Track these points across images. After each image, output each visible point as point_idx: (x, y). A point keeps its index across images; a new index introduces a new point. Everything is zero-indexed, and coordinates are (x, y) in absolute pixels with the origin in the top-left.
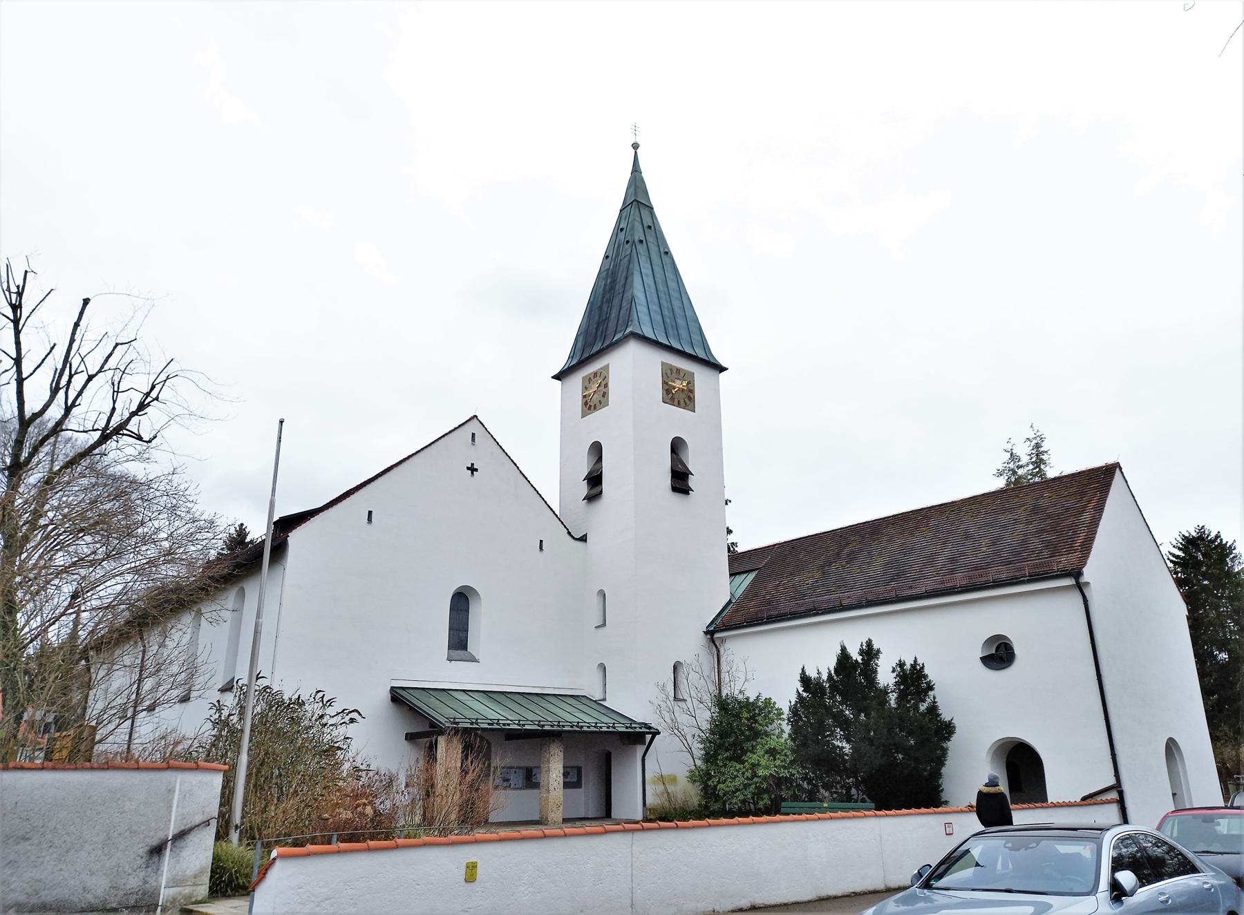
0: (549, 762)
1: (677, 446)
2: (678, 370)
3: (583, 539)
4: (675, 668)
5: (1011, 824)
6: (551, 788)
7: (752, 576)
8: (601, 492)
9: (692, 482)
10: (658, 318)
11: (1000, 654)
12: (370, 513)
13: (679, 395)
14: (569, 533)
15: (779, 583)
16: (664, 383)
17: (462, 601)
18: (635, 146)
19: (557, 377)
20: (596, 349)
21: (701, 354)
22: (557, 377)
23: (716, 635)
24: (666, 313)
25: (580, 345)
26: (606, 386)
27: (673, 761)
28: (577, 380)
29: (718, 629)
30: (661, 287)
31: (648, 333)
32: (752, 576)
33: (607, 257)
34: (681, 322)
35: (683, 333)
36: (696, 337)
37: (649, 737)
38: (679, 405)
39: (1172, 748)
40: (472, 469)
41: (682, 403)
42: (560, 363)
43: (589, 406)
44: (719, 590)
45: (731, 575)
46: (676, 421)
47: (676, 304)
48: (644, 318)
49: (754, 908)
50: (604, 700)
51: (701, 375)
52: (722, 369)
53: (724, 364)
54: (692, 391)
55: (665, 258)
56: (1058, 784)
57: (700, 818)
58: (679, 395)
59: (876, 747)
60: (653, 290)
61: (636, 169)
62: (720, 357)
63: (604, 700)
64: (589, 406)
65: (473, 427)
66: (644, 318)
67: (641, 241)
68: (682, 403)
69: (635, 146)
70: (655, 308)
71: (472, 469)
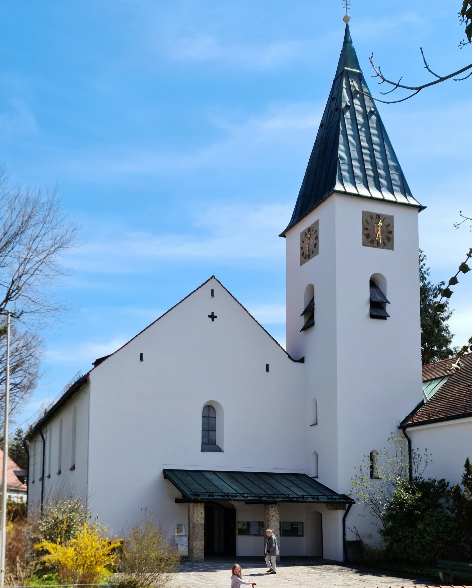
3: (302, 360)
5: (277, 566)
8: (313, 324)
9: (389, 309)
14: (290, 357)
16: (365, 229)
17: (267, 366)
19: (283, 235)
22: (283, 235)
23: (408, 430)
26: (317, 238)
27: (362, 523)
37: (347, 505)
38: (378, 245)
40: (213, 317)
46: (376, 260)
50: (317, 477)
56: (242, 523)
58: (378, 233)
61: (347, 41)
63: (317, 477)
65: (213, 285)
69: (346, 19)
71: (213, 317)
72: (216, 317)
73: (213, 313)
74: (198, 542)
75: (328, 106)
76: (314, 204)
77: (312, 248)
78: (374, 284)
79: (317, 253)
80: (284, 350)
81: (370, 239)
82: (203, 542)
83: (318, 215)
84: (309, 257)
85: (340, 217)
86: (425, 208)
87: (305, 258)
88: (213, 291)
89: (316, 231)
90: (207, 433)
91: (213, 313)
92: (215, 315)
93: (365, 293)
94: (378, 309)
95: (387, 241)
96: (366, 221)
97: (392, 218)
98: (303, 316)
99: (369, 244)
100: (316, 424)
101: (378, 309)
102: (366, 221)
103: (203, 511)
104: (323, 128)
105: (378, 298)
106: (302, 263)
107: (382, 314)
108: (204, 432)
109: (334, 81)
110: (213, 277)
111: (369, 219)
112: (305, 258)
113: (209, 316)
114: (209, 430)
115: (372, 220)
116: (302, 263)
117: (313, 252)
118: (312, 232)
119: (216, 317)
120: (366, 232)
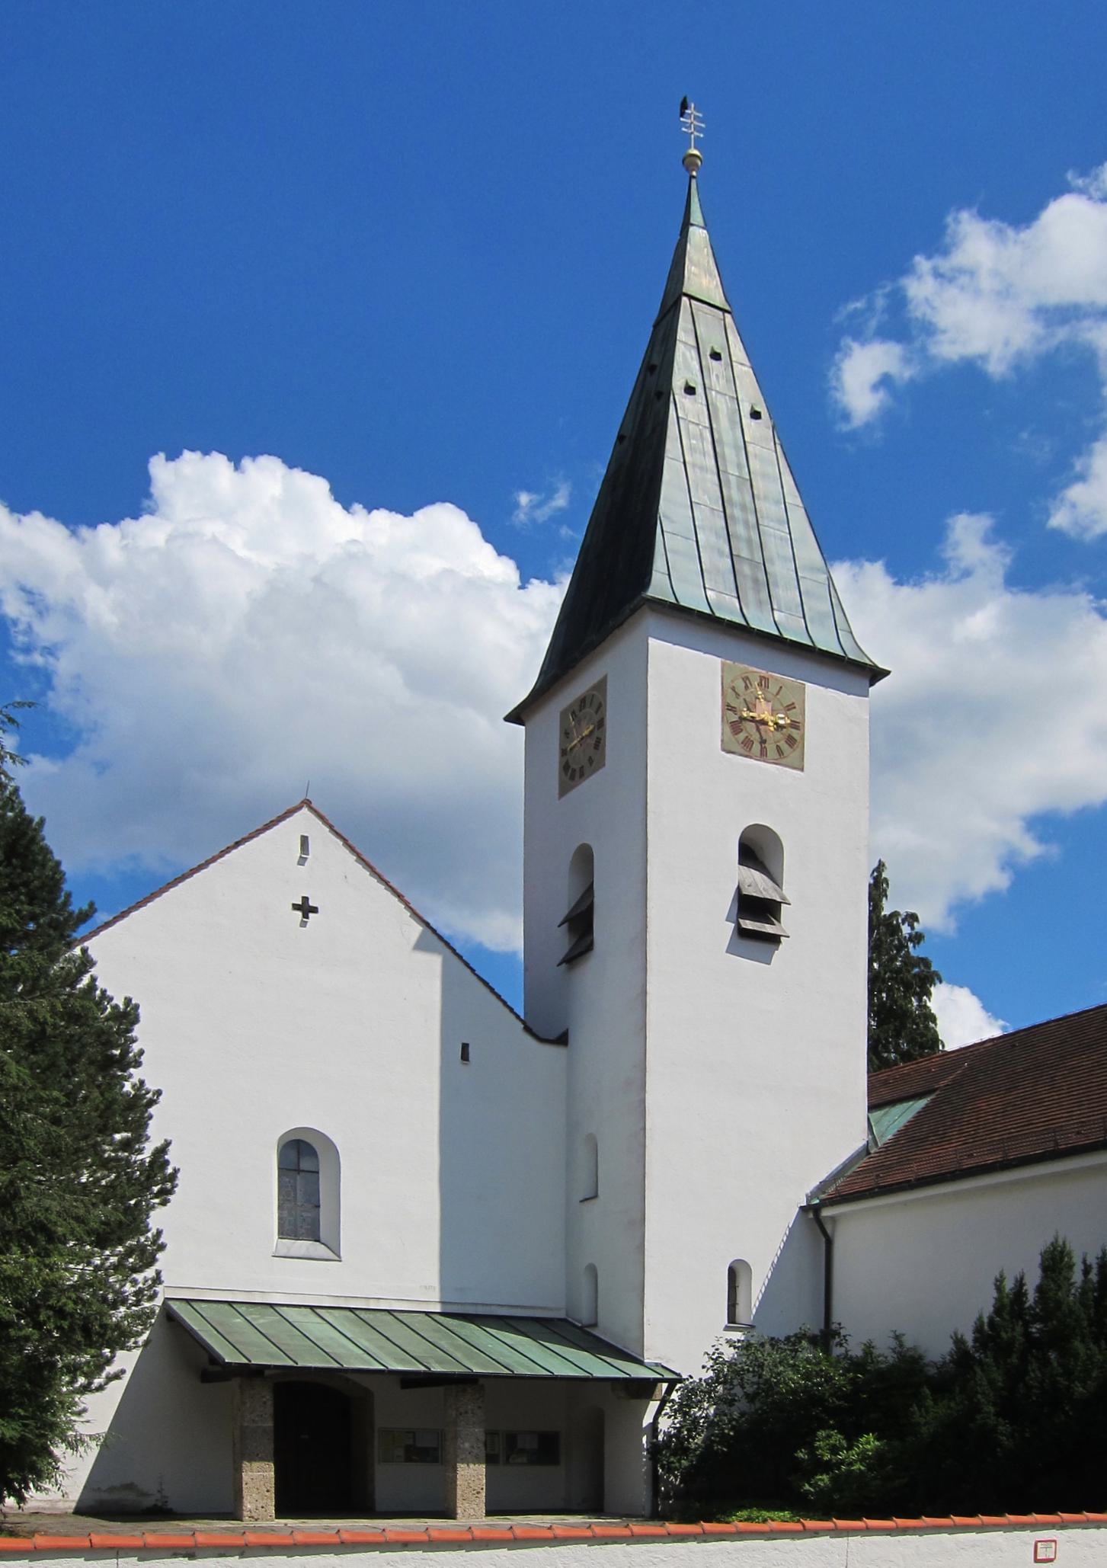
3: (562, 1040)
4: (732, 1273)
7: (921, 1104)
8: (590, 947)
9: (788, 921)
14: (528, 1029)
17: (465, 1047)
19: (516, 717)
21: (826, 642)
22: (516, 717)
23: (826, 1212)
26: (601, 724)
30: (733, 493)
31: (692, 598)
32: (921, 1104)
33: (621, 438)
37: (665, 1386)
40: (305, 908)
45: (872, 1108)
46: (759, 791)
57: (826, 1516)
63: (595, 1325)
67: (690, 390)
70: (712, 539)
71: (305, 908)
72: (315, 910)
73: (305, 899)
75: (520, 1326)
76: (640, 1362)
78: (756, 850)
80: (518, 1017)
87: (572, 778)
89: (600, 707)
91: (305, 899)
92: (311, 903)
94: (756, 920)
95: (784, 744)
96: (733, 689)
98: (565, 926)
99: (738, 748)
100: (596, 1196)
101: (756, 920)
102: (733, 689)
103: (268, 1397)
104: (626, 443)
105: (758, 884)
106: (563, 791)
109: (655, 326)
110: (1037, 1561)
112: (572, 778)
113: (296, 907)
115: (746, 687)
116: (563, 791)
117: (591, 760)
118: (592, 705)
119: (315, 910)
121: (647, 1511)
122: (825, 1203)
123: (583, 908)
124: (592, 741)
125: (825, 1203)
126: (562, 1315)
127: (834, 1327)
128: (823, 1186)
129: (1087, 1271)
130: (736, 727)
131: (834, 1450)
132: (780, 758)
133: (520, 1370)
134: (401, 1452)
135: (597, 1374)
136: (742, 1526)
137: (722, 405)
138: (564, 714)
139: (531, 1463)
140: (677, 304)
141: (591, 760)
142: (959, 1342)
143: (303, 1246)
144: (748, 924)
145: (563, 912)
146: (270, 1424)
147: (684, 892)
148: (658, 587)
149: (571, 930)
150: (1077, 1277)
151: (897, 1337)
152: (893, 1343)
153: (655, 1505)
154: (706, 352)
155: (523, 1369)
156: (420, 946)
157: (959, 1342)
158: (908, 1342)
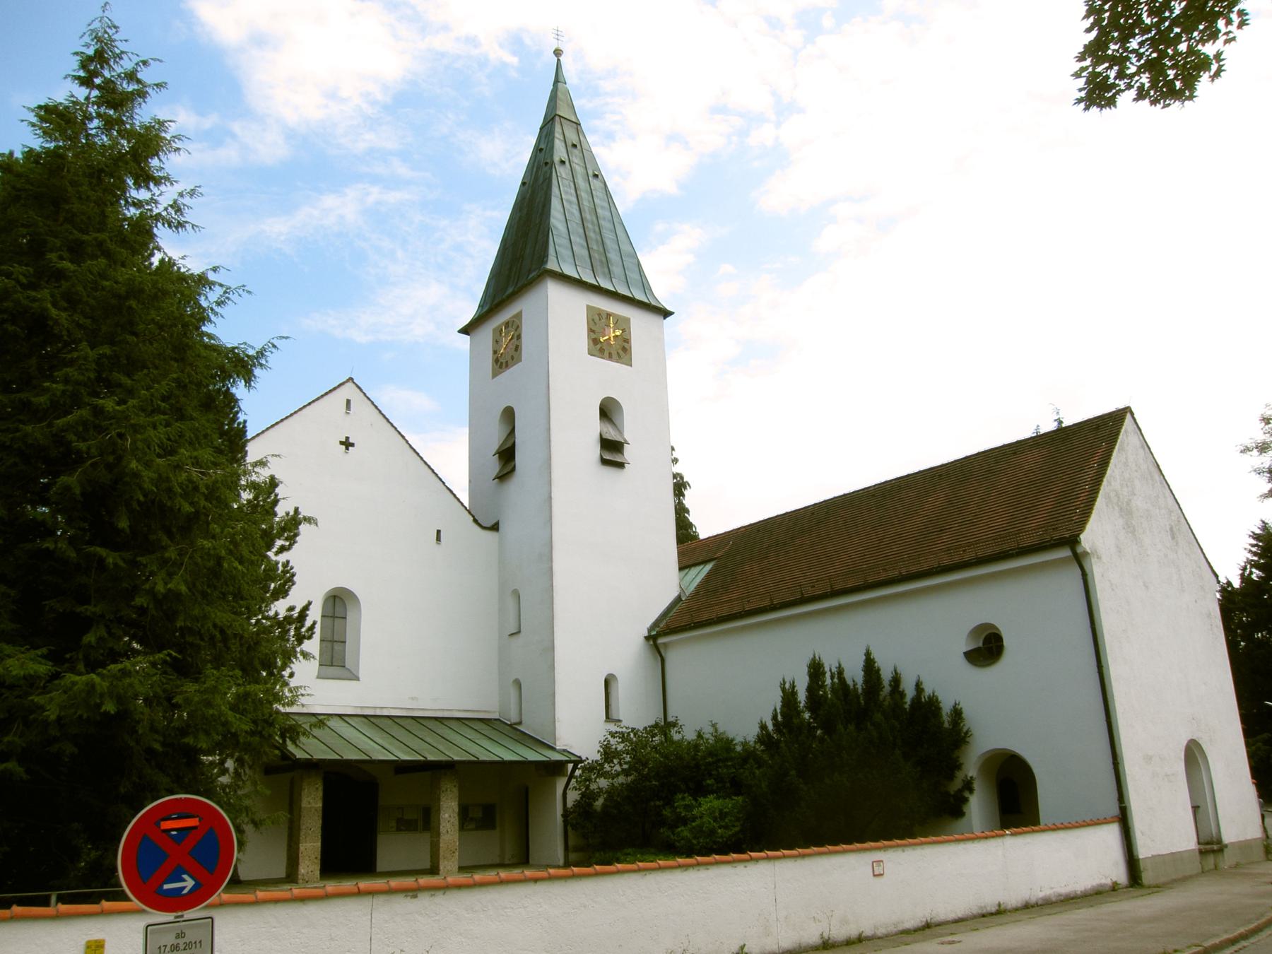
0: (439, 800)
1: (608, 411)
2: (609, 315)
3: (495, 527)
4: (607, 683)
6: (443, 830)
7: (709, 567)
8: (513, 469)
9: (629, 453)
10: (581, 251)
11: (988, 648)
12: (439, 532)
13: (610, 345)
14: (475, 521)
15: (741, 576)
16: (591, 331)
17: (439, 532)
18: (558, 53)
19: (465, 331)
20: (510, 290)
21: (639, 296)
22: (465, 331)
23: (661, 641)
24: (594, 246)
25: (491, 290)
26: (519, 337)
28: (486, 333)
29: (669, 629)
30: (587, 216)
31: (569, 270)
32: (709, 567)
33: (523, 184)
34: (613, 256)
35: (617, 270)
36: (633, 276)
37: (570, 766)
38: (610, 357)
39: (1194, 755)
40: (347, 444)
41: (615, 355)
42: (469, 312)
43: (502, 363)
44: (662, 582)
45: (681, 569)
46: (607, 378)
47: (608, 235)
48: (565, 252)
49: (826, 945)
51: (639, 322)
52: (666, 314)
53: (669, 308)
54: (627, 341)
55: (594, 182)
57: (689, 855)
58: (610, 345)
59: (868, 767)
60: (578, 220)
61: (558, 79)
62: (662, 296)
64: (502, 363)
65: (348, 392)
66: (565, 252)
67: (563, 162)
68: (615, 355)
69: (558, 53)
70: (578, 240)
71: (347, 444)
72: (352, 445)
73: (347, 438)
74: (308, 845)
76: (553, 749)
77: (512, 352)
78: (608, 411)
79: (520, 360)
81: (598, 347)
82: (319, 844)
83: (526, 306)
84: (507, 366)
85: (560, 313)
86: (671, 313)
87: (501, 367)
88: (348, 402)
90: (329, 645)
91: (347, 438)
93: (594, 427)
95: (619, 351)
97: (628, 320)
100: (519, 632)
101: (612, 452)
103: (320, 786)
105: (612, 434)
106: (494, 375)
107: (618, 459)
108: (325, 644)
110: (351, 379)
111: (597, 318)
112: (501, 367)
113: (342, 443)
114: (333, 641)
116: (494, 375)
117: (513, 358)
118: (514, 326)
119: (352, 445)
120: (593, 336)
121: (561, 862)
122: (659, 635)
123: (509, 444)
124: (512, 347)
125: (659, 635)
126: (496, 716)
127: (670, 719)
128: (656, 624)
129: (832, 677)
130: (595, 341)
131: (688, 808)
132: (619, 359)
133: (482, 758)
134: (394, 824)
135: (531, 758)
136: (225, 897)
137: (579, 170)
138: (494, 330)
139: (477, 829)
140: (553, 119)
141: (513, 358)
142: (763, 727)
143: (331, 670)
144: (608, 456)
145: (495, 446)
146: (320, 805)
147: (574, 437)
148: (552, 265)
149: (500, 458)
150: (828, 681)
151: (714, 726)
152: (711, 730)
153: (566, 857)
154: (569, 144)
155: (484, 757)
156: (1086, 554)
157: (763, 727)
158: (721, 730)
